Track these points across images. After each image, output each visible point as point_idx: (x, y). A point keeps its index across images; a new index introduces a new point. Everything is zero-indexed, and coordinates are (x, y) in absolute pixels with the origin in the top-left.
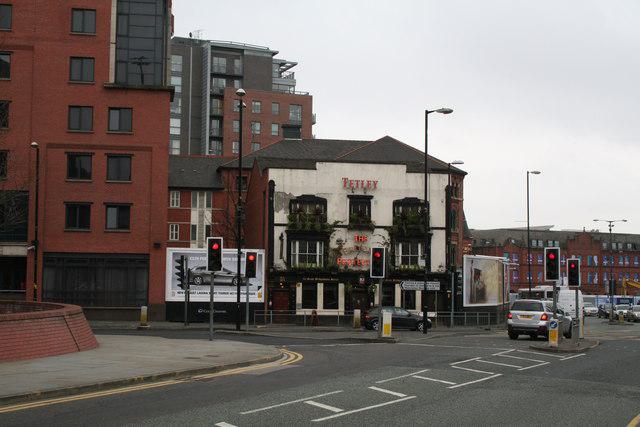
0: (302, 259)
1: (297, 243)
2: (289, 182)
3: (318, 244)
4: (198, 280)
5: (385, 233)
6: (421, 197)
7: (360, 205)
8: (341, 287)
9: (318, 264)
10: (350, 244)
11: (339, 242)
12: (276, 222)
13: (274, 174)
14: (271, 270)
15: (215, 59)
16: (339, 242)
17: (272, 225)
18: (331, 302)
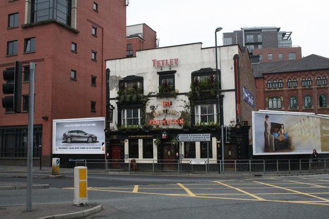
0: (129, 122)
1: (126, 111)
2: (120, 68)
4: (69, 140)
5: (186, 98)
6: (213, 67)
9: (140, 125)
10: (160, 109)
11: (153, 108)
13: (109, 65)
15: (248, 36)
16: (153, 108)
17: (108, 99)
18: (148, 153)
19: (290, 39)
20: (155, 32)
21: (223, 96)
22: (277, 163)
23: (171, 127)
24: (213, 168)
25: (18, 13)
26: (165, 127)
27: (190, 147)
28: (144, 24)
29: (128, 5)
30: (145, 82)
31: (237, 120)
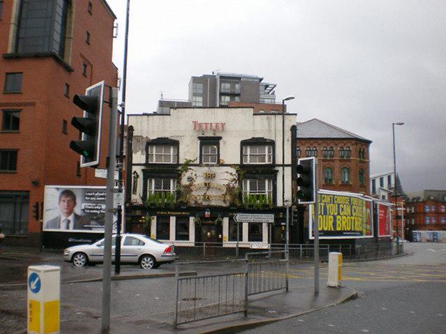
3: (172, 181)
5: (233, 171)
7: (210, 142)
8: (192, 220)
11: (190, 179)
12: (133, 162)
14: (128, 205)
15: (223, 85)
16: (190, 179)
17: (130, 164)
19: (273, 93)
20: (117, 69)
23: (213, 203)
24: (259, 254)
25: (293, 98)
26: (205, 203)
27: (255, 232)
29: (116, 37)
30: (181, 147)
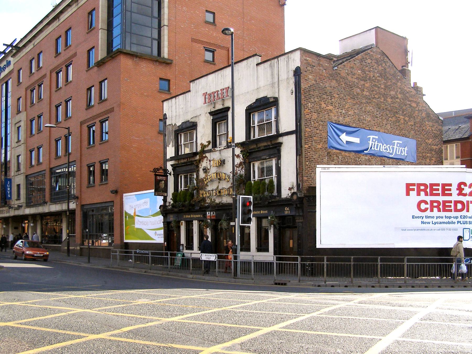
11: (206, 170)
21: (281, 143)
22: (325, 263)
24: (264, 268)
28: (377, 28)
31: (298, 185)
